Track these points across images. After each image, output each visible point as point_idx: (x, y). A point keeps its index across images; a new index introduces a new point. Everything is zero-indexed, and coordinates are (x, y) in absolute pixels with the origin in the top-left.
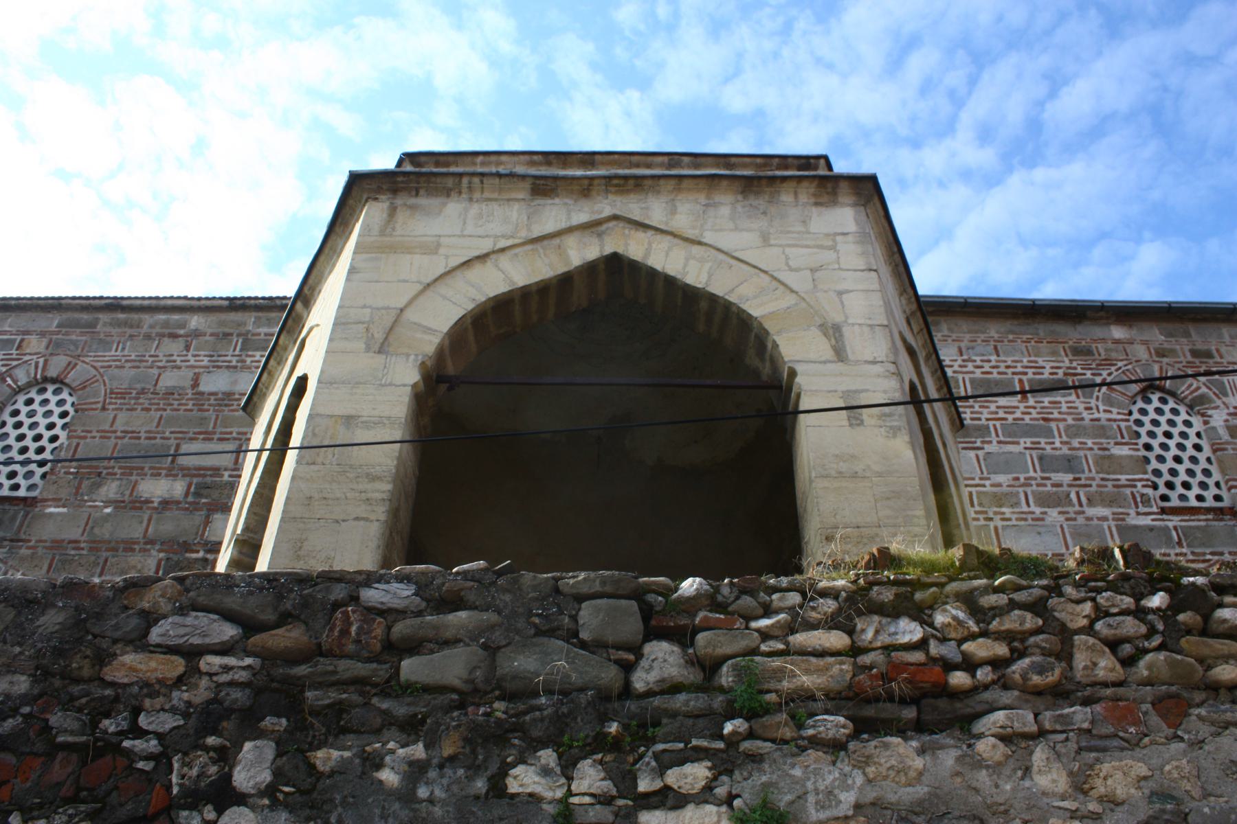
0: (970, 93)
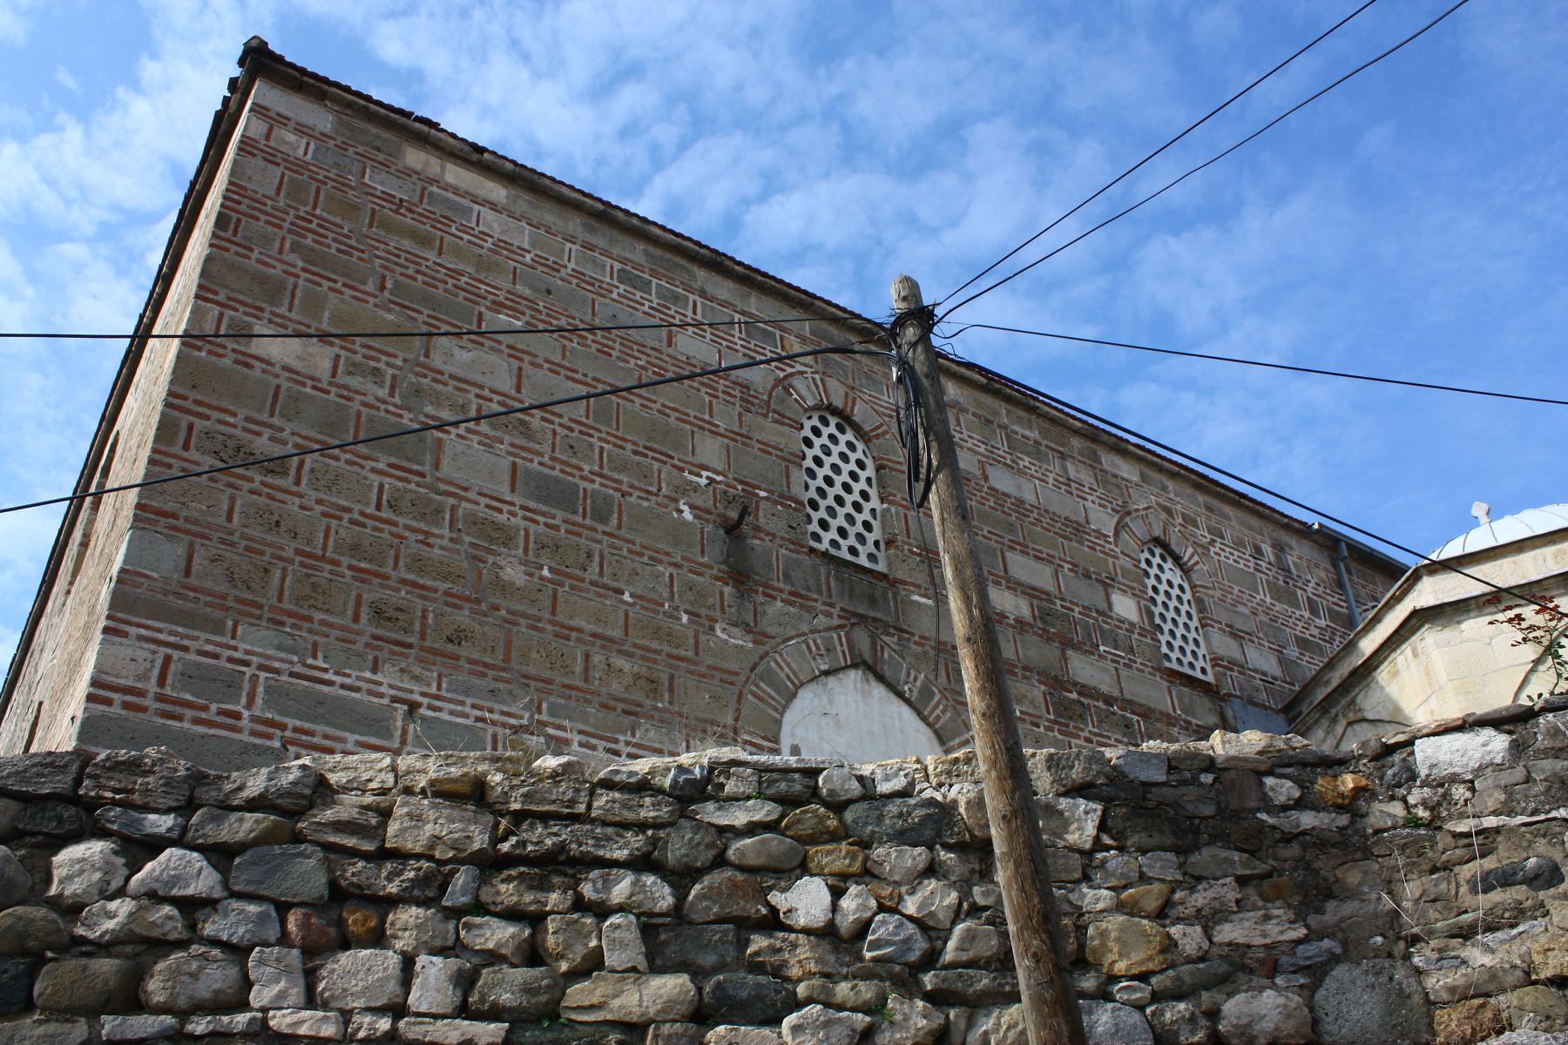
0: (675, 158)
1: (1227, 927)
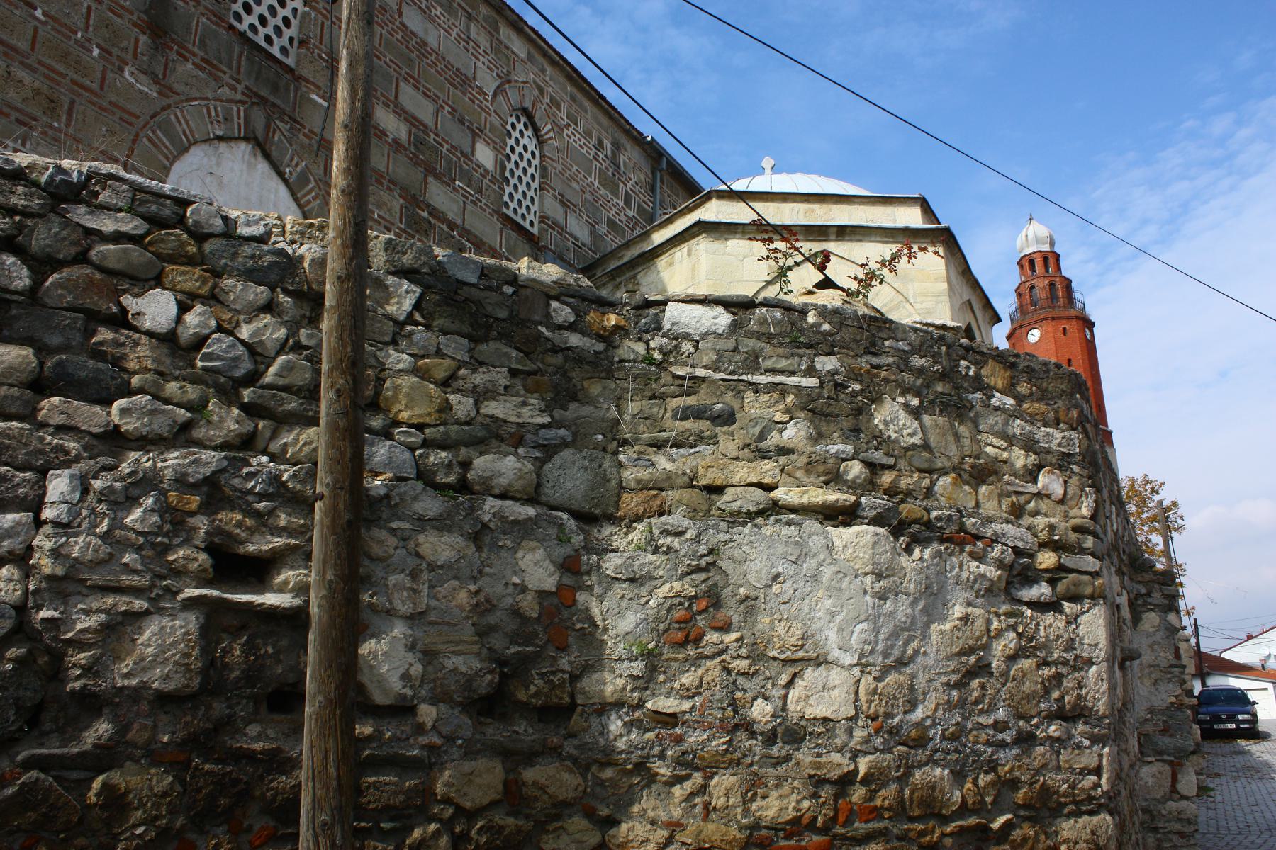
1: (493, 404)
